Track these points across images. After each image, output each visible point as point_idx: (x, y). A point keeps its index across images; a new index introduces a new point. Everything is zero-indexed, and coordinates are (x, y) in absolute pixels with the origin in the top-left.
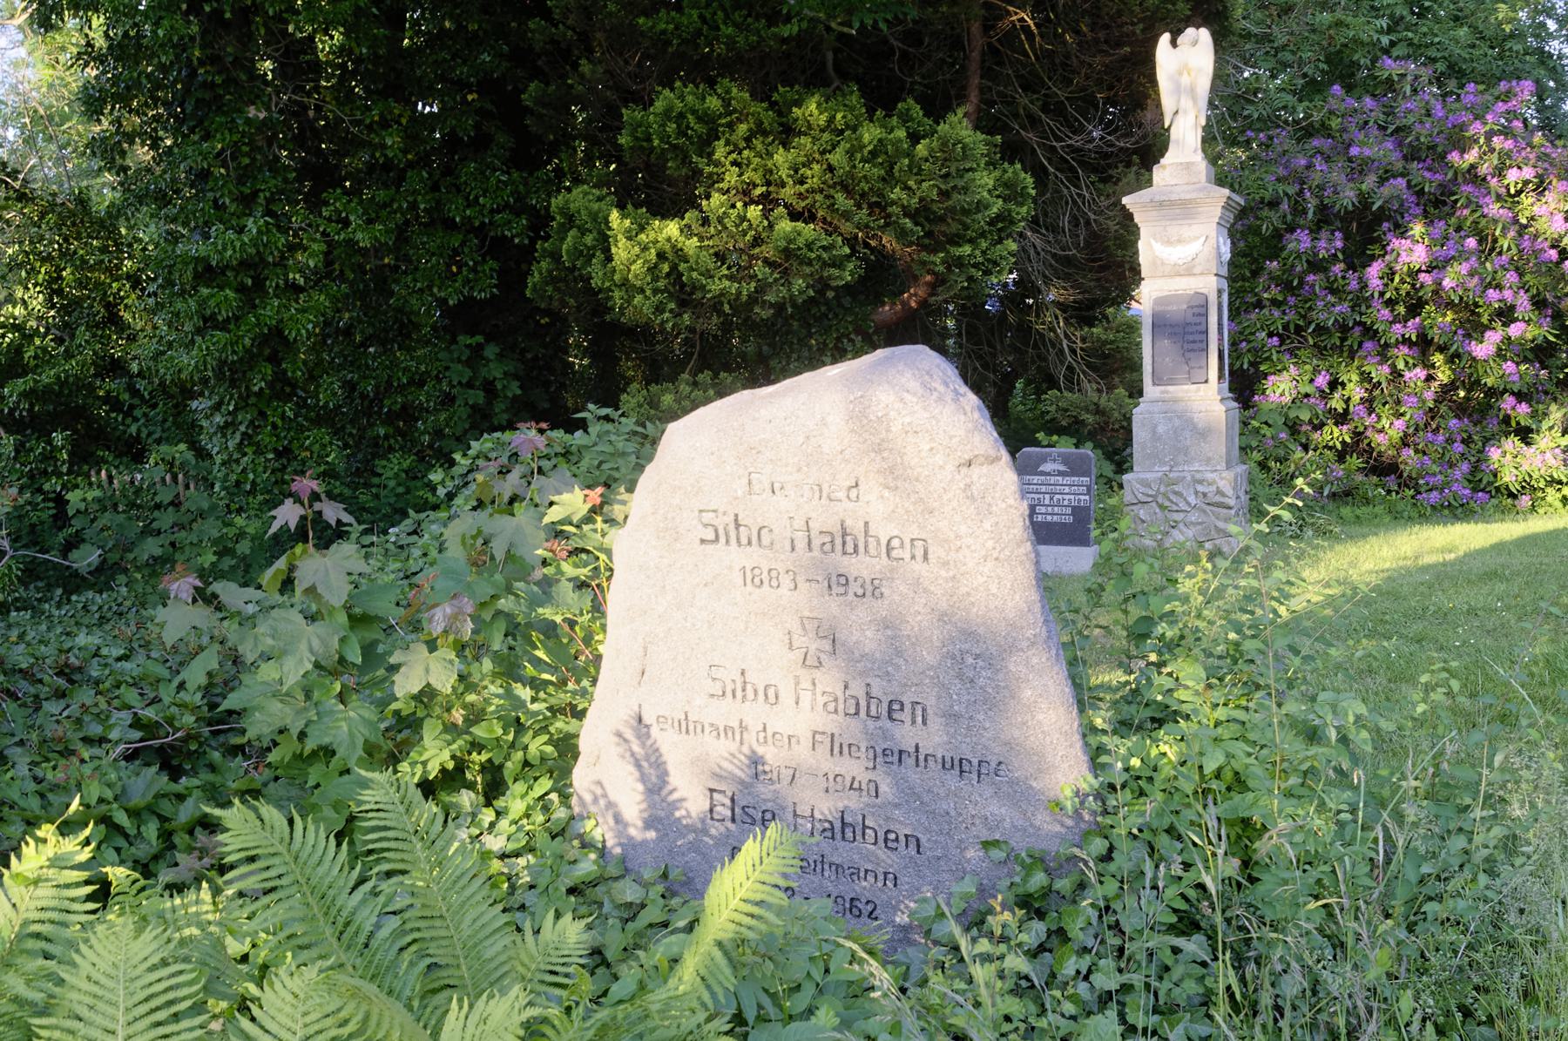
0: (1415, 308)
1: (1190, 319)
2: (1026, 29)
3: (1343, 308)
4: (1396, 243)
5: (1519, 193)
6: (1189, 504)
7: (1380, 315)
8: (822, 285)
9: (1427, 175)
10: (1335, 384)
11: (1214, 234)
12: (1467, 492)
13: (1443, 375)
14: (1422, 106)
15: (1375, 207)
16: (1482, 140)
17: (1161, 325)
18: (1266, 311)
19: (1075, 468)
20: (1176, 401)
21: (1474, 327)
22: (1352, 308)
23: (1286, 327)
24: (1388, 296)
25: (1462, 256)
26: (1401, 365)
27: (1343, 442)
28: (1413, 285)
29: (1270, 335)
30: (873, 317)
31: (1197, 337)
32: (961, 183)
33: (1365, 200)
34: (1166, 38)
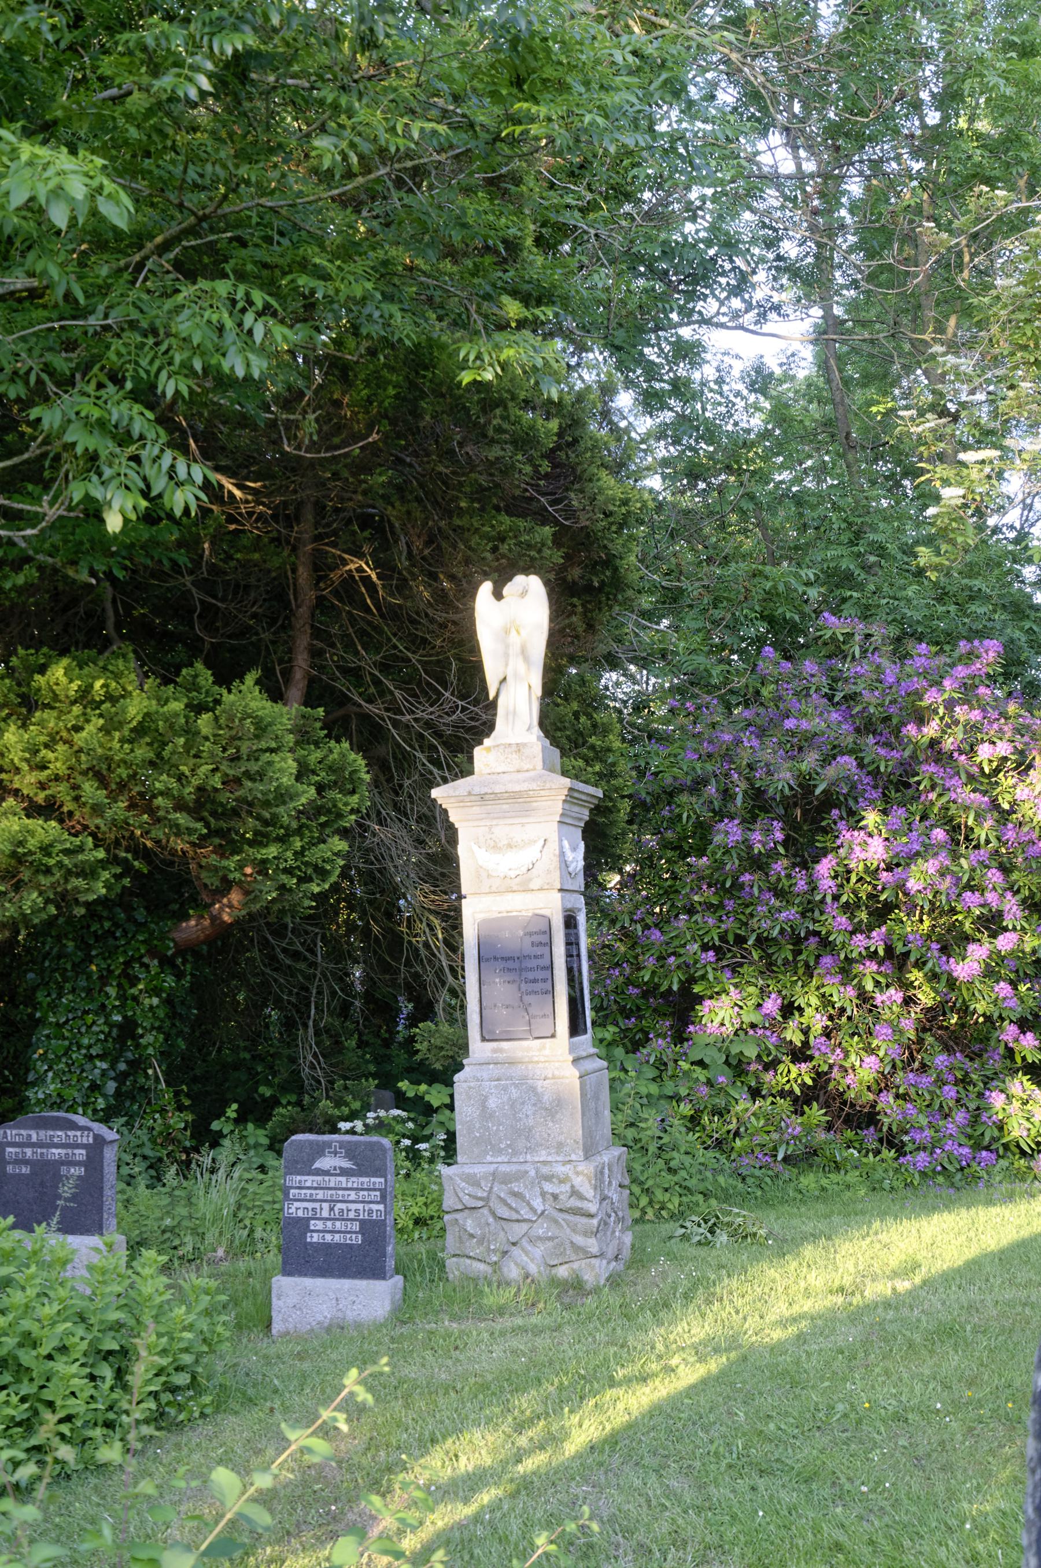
0: (882, 912)
1: (528, 949)
3: (790, 914)
4: (846, 836)
5: (996, 771)
6: (533, 1210)
8: (64, 899)
9: (882, 752)
10: (789, 1009)
11: (554, 837)
12: (965, 1151)
13: (926, 997)
14: (872, 674)
15: (818, 792)
16: (941, 711)
18: (697, 917)
21: (953, 942)
22: (803, 915)
23: (723, 938)
24: (844, 899)
26: (869, 986)
27: (804, 1084)
28: (875, 887)
29: (705, 948)
30: (175, 935)
31: (540, 975)
32: (254, 767)
33: (806, 783)
34: (486, 588)
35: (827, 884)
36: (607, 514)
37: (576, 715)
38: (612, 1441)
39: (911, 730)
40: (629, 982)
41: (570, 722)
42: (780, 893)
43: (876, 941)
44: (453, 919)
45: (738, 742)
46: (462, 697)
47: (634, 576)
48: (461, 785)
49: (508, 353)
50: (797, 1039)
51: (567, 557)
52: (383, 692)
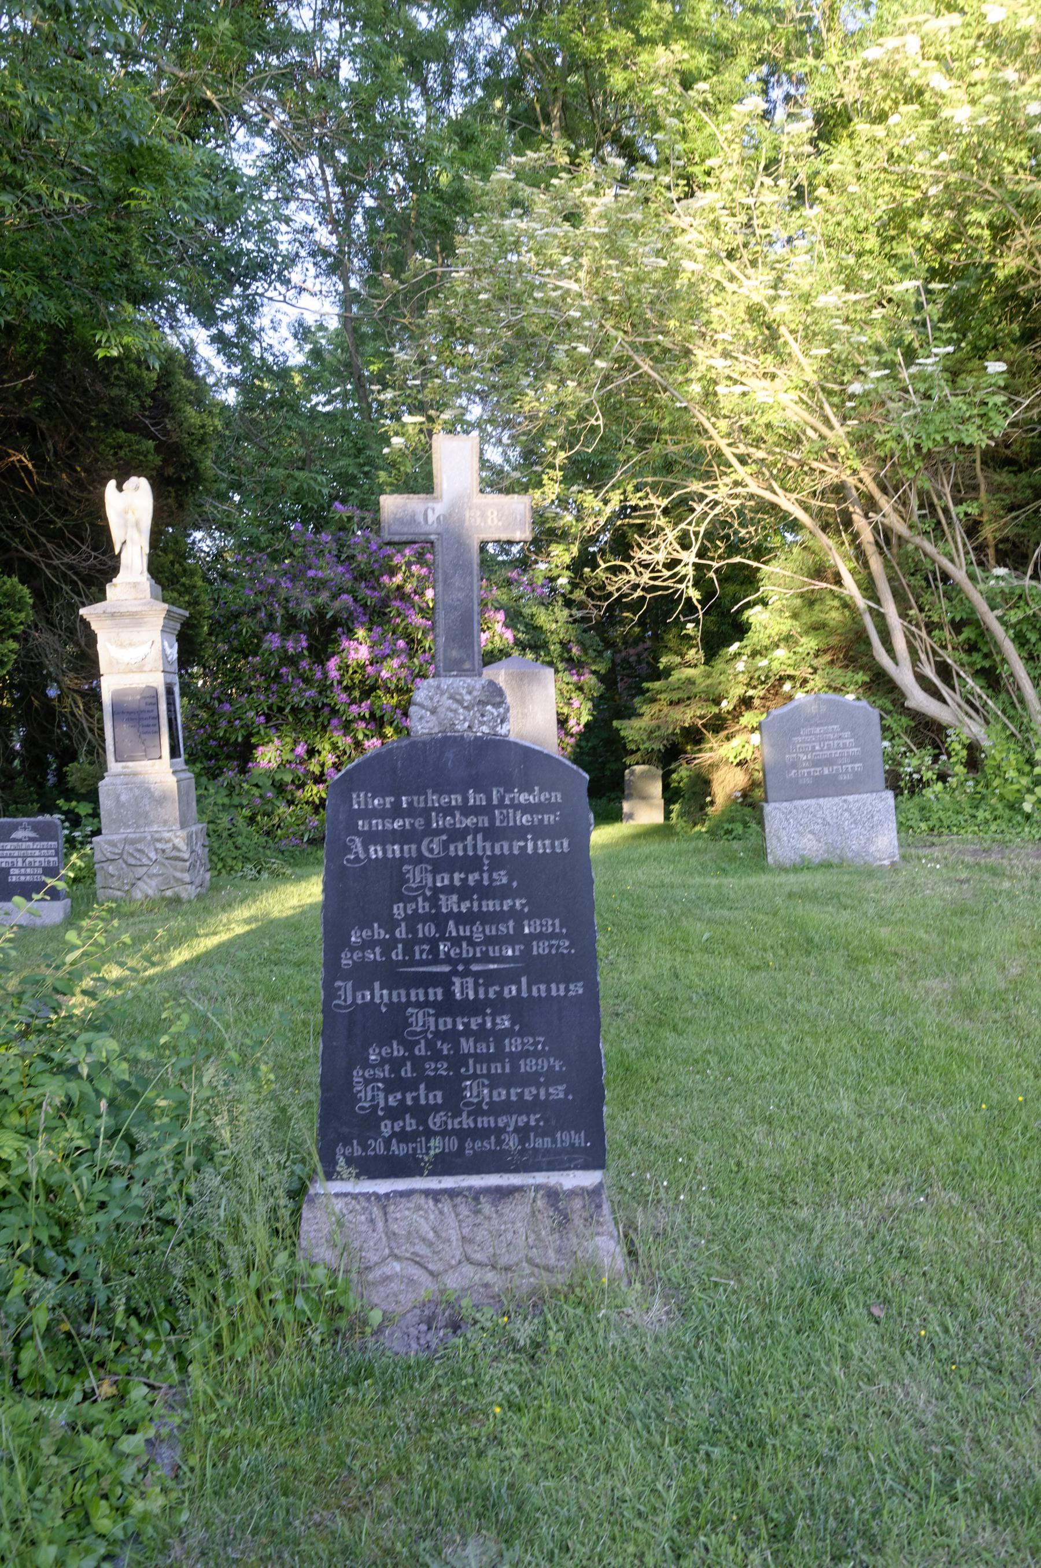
0: (369, 690)
1: (143, 706)
2: (25, 468)
3: (312, 693)
4: (345, 644)
7: (340, 697)
10: (312, 752)
17: (120, 712)
19: (44, 833)
20: (135, 774)
23: (270, 708)
25: (394, 653)
26: (360, 737)
34: (112, 483)
35: (334, 674)
36: (190, 434)
37: (172, 563)
38: (198, 959)
39: (385, 579)
40: (210, 737)
41: (168, 567)
42: (307, 681)
43: (364, 709)
44: (94, 696)
45: (278, 584)
46: (95, 549)
47: (210, 474)
48: (99, 607)
49: (126, 340)
50: (317, 770)
51: (164, 460)
52: (38, 545)
